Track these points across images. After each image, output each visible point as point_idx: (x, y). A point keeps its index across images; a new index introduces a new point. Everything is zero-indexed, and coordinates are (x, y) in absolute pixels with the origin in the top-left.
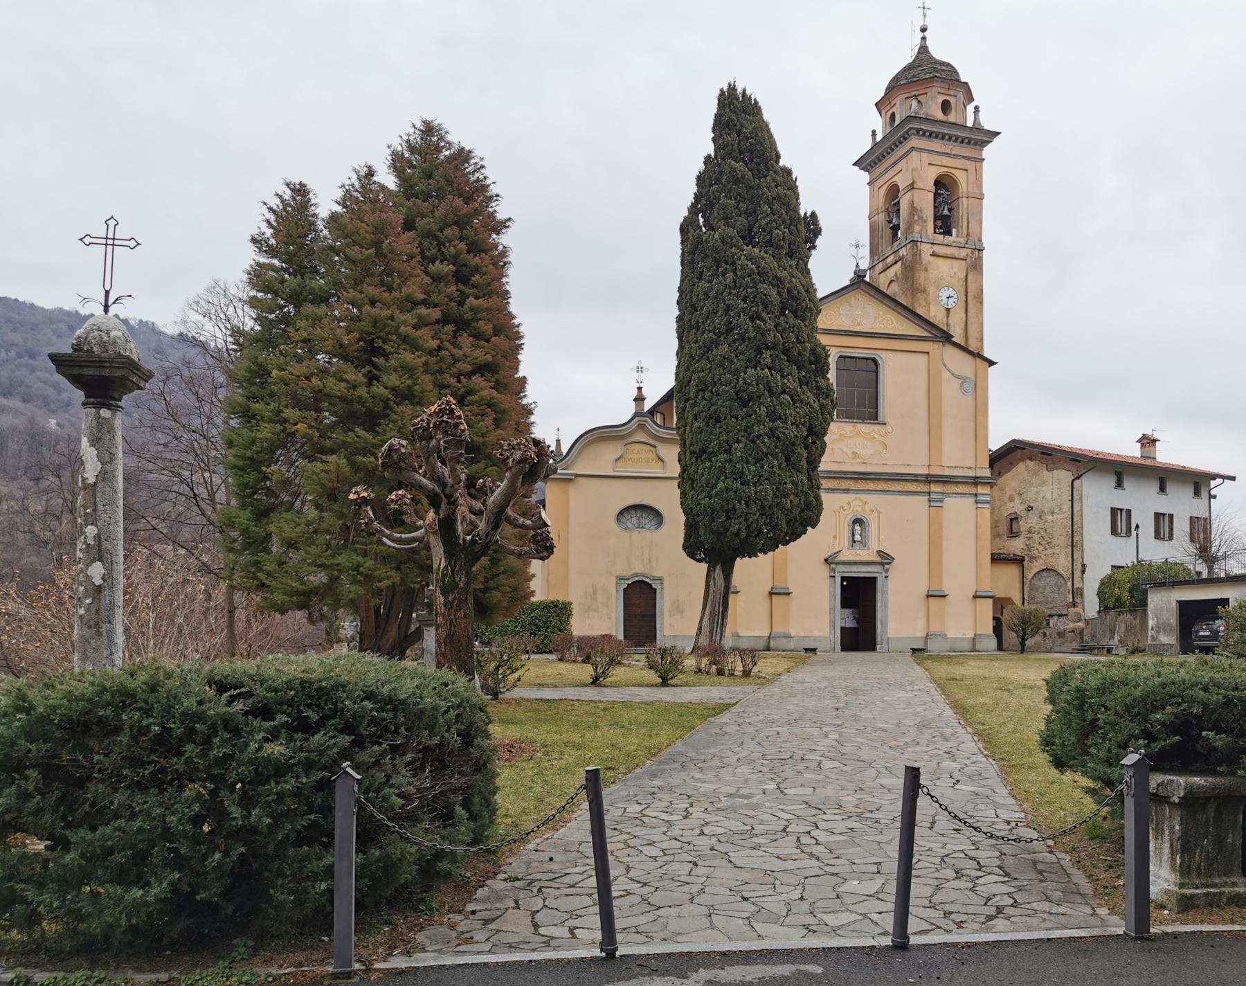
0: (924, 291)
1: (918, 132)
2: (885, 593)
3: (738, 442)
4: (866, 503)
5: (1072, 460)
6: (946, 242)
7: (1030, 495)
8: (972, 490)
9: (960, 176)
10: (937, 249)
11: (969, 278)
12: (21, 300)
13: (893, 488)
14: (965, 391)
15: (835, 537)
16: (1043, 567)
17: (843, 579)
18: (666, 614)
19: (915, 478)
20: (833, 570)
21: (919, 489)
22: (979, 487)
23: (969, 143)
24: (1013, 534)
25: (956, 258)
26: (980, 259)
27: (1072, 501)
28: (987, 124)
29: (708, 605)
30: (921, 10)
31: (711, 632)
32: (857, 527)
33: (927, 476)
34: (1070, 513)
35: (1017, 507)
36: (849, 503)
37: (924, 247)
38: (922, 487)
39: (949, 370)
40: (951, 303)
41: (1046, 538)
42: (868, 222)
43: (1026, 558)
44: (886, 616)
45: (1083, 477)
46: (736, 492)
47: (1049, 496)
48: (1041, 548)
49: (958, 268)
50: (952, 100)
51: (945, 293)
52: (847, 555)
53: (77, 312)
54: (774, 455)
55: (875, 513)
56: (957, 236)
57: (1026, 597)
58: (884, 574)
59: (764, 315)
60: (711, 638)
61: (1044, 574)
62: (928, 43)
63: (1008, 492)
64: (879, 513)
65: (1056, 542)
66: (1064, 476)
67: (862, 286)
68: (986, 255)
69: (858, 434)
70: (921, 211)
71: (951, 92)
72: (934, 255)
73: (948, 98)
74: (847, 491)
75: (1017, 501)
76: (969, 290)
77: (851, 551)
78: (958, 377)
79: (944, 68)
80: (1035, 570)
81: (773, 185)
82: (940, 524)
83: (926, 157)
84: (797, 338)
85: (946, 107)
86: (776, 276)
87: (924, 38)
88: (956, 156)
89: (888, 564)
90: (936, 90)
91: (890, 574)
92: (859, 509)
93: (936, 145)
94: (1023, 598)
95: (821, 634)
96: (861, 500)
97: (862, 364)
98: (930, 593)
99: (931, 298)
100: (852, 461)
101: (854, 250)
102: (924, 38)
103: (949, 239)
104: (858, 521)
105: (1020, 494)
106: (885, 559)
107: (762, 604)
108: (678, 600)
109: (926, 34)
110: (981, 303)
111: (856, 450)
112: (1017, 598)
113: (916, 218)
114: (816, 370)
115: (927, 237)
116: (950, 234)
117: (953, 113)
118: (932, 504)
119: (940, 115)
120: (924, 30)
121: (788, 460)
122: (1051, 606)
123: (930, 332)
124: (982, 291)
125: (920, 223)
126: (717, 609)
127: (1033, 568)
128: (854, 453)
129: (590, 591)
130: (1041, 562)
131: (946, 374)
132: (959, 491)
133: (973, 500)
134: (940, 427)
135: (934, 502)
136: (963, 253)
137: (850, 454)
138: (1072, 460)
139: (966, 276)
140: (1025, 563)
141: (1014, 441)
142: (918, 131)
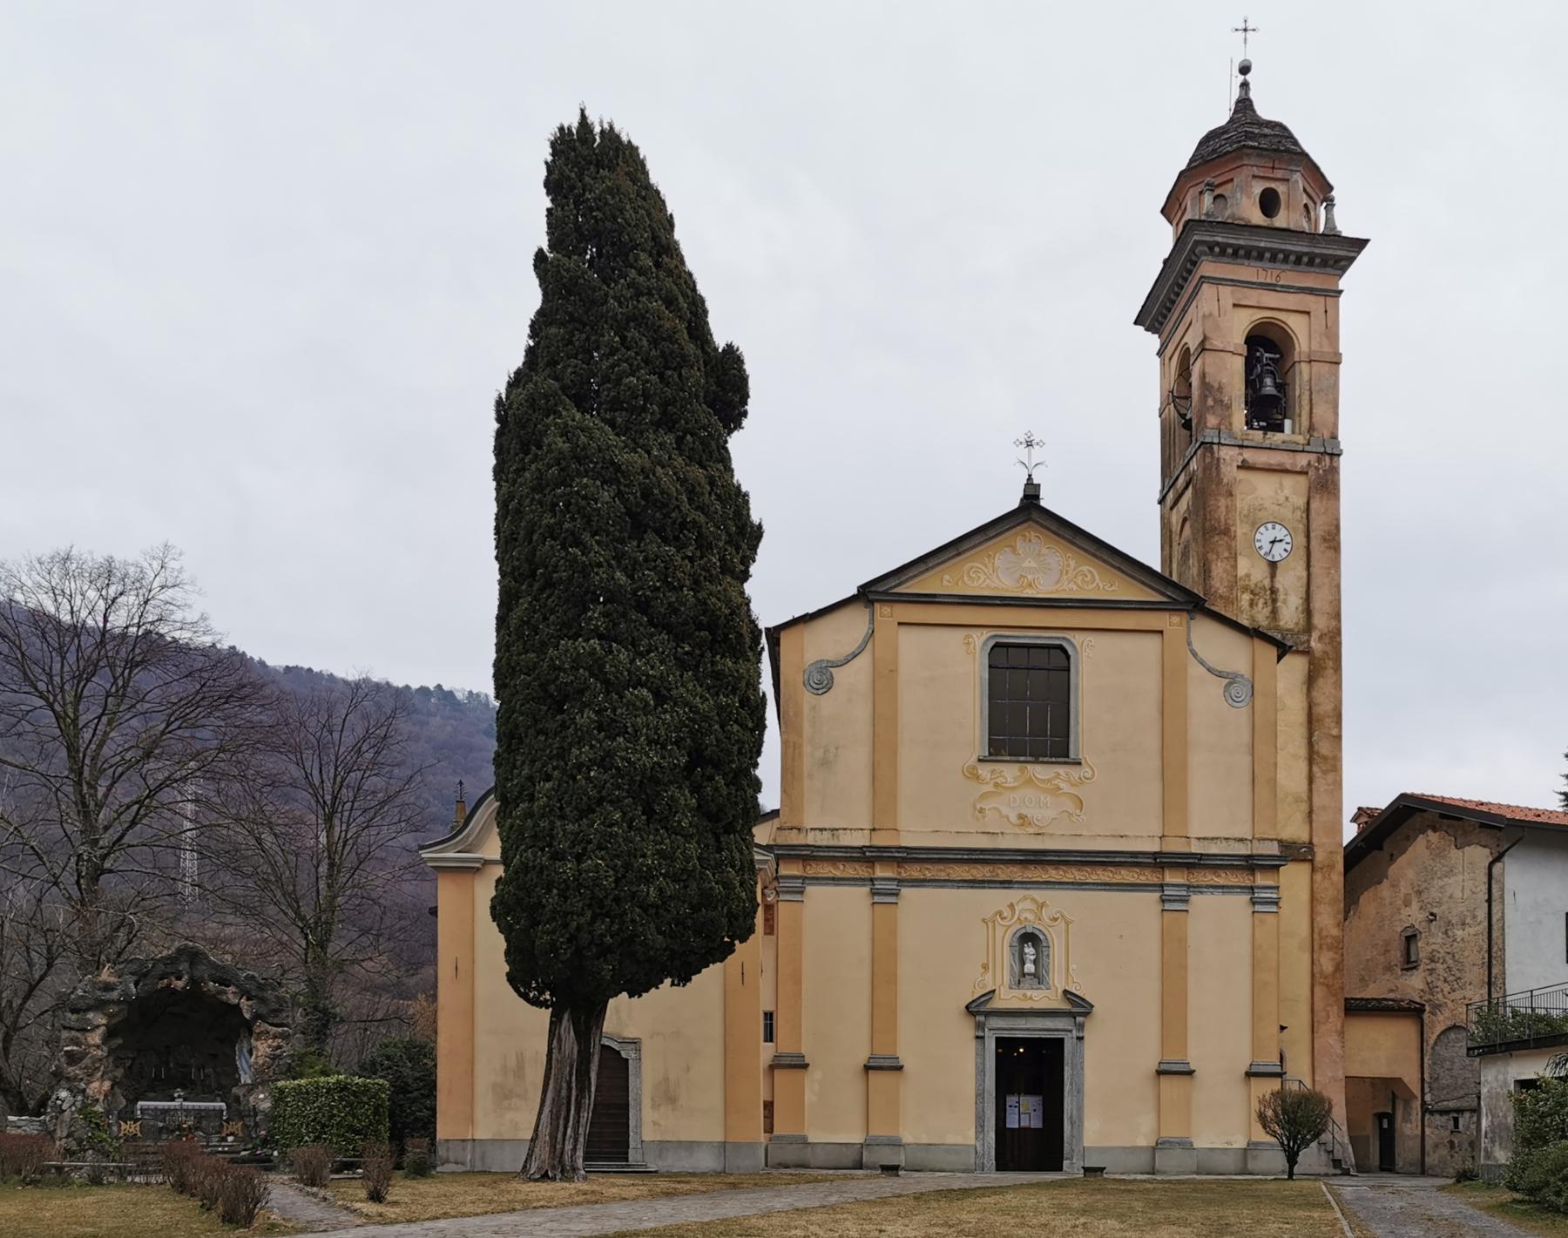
0: (1226, 532)
1: (1211, 249)
2: (1079, 1068)
3: (548, 778)
4: (1042, 905)
5: (1483, 826)
6: (1267, 443)
7: (1434, 894)
8: (1245, 880)
9: (1296, 324)
10: (1249, 455)
11: (1314, 505)
12: (316, 669)
13: (1093, 878)
14: (1232, 700)
15: (985, 967)
16: (1450, 1023)
17: (998, 1040)
18: (646, 1102)
19: (1133, 860)
20: (980, 1026)
21: (1142, 879)
22: (1167, 873)
23: (1311, 263)
24: (1410, 964)
25: (1286, 471)
26: (1334, 470)
27: (1489, 901)
28: (1347, 226)
29: (551, 1087)
30: (1241, 34)
31: (553, 1137)
32: (1029, 950)
33: (1155, 855)
34: (1486, 924)
35: (1414, 915)
36: (1012, 906)
37: (1226, 454)
38: (862, 871)
39: (1202, 663)
40: (1278, 552)
41: (1455, 971)
42: (1158, 421)
43: (1427, 1008)
44: (1080, 1109)
45: (1506, 859)
46: (541, 872)
47: (1458, 894)
48: (1447, 988)
49: (1292, 490)
50: (1281, 188)
51: (1265, 536)
52: (1008, 998)
53: (388, 683)
54: (616, 802)
55: (1061, 924)
56: (1293, 432)
57: (1426, 1076)
58: (1075, 1033)
59: (586, 537)
60: (553, 1146)
61: (1452, 1035)
62: (1252, 95)
63: (1404, 888)
64: (1067, 923)
65: (1468, 977)
66: (1478, 855)
67: (1035, 515)
68: (1344, 463)
69: (1029, 782)
70: (1220, 389)
71: (1279, 174)
72: (1245, 466)
73: (1273, 185)
74: (1007, 884)
75: (1415, 905)
76: (1313, 526)
77: (1018, 993)
78: (1220, 674)
79: (1266, 131)
80: (1439, 1029)
81: (628, 293)
82: (1183, 942)
83: (1227, 293)
84: (665, 581)
85: (1269, 203)
86: (612, 463)
87: (1245, 86)
88: (1288, 289)
89: (1081, 1014)
90: (1247, 171)
91: (1086, 1034)
92: (1031, 917)
93: (1247, 272)
94: (1423, 1080)
95: (958, 1140)
96: (1033, 900)
97: (1038, 658)
98: (1163, 1067)
99: (1240, 544)
100: (1017, 830)
101: (1023, 452)
102: (1245, 86)
103: (1277, 438)
104: (1029, 938)
105: (1419, 893)
106: (1078, 1008)
107: (850, 1091)
108: (667, 1079)
109: (1249, 77)
110: (1336, 549)
111: (1024, 811)
112: (1411, 1079)
113: (1210, 402)
114: (714, 641)
115: (1231, 435)
116: (1280, 429)
117: (1282, 213)
118: (1167, 906)
119: (1257, 217)
120: (1245, 70)
121: (649, 812)
122: (1462, 1093)
123: (1163, 594)
124: (1338, 527)
125: (1219, 411)
126: (564, 1093)
127: (1437, 1024)
128: (1021, 817)
129: (512, 1062)
130: (1447, 1013)
131: (1196, 670)
132: (1221, 881)
133: (1246, 898)
134: (1184, 768)
135: (1175, 903)
136: (1302, 461)
137: (1013, 818)
138: (1483, 826)
139: (1308, 503)
140: (1426, 1016)
141: (1403, 796)
142: (1211, 246)
